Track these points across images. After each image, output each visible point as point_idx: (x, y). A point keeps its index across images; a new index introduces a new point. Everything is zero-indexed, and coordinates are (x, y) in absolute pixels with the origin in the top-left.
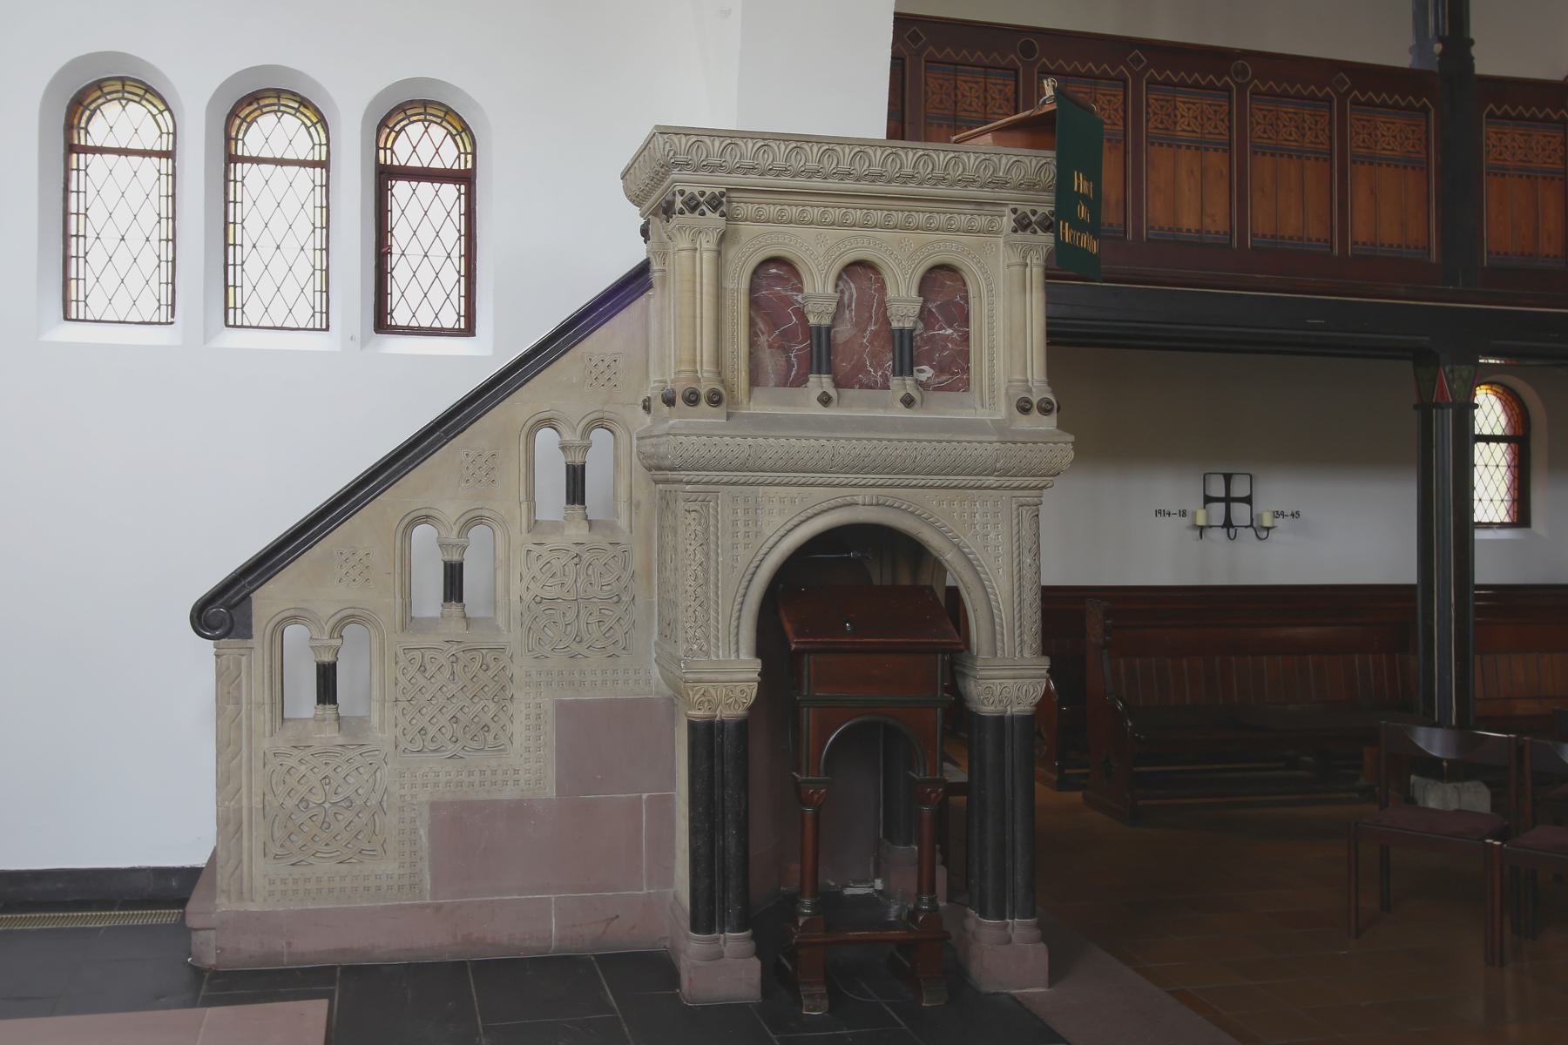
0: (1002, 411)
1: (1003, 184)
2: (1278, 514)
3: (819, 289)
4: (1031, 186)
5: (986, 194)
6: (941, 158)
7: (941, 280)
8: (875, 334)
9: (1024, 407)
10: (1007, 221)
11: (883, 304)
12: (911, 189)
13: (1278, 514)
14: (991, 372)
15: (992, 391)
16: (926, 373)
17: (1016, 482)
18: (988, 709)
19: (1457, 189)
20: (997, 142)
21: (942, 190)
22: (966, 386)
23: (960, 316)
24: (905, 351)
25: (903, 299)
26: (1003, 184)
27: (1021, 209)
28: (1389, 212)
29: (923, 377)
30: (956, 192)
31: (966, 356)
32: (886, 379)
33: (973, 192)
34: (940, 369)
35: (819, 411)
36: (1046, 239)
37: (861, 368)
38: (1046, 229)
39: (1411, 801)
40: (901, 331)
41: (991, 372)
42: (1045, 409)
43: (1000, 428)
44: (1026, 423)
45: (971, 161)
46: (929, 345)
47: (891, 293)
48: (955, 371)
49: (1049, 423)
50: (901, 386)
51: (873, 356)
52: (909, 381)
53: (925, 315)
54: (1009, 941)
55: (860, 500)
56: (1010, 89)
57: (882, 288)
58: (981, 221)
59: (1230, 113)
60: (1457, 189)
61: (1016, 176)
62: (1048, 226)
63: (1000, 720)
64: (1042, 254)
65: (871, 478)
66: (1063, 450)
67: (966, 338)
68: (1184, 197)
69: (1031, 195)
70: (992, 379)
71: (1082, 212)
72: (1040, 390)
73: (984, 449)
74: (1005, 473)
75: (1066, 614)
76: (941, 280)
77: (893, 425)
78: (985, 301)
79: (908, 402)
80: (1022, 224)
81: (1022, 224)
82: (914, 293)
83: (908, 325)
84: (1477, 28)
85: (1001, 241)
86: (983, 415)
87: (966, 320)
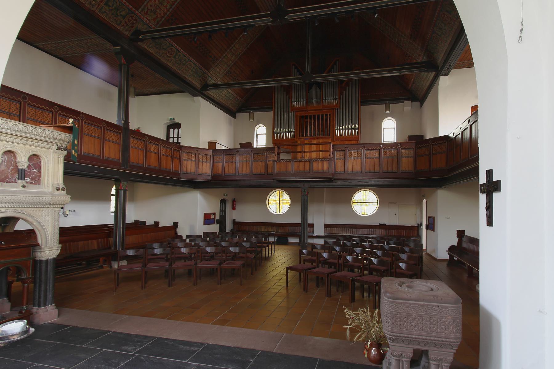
0: (50, 190)
1: (55, 139)
2: (70, 211)
3: (23, 160)
4: (62, 140)
5: (50, 140)
6: (39, 130)
7: (34, 159)
8: (13, 169)
9: (58, 189)
10: (55, 147)
11: (15, 162)
12: (29, 136)
13: (70, 211)
14: (48, 181)
15: (48, 185)
16: (28, 180)
17: (56, 206)
18: (44, 258)
19: (126, 149)
20: (54, 129)
21: (38, 137)
22: (39, 183)
23: (39, 167)
24: (22, 174)
25: (23, 162)
26: (55, 139)
27: (59, 145)
28: (112, 152)
29: (27, 181)
30: (42, 138)
31: (40, 177)
32: (16, 180)
33: (47, 139)
34: (32, 179)
35: (22, 189)
36: (65, 153)
37: (8, 177)
38: (65, 150)
39: (111, 267)
40: (22, 169)
41: (48, 181)
42: (63, 190)
43: (52, 194)
44: (58, 193)
45: (48, 132)
46: (31, 172)
47: (18, 159)
48: (37, 180)
49: (64, 193)
50: (21, 183)
51: (12, 175)
52: (24, 181)
53: (29, 167)
54: (47, 311)
55: (8, 211)
56: (18, 106)
57: (15, 158)
58: (48, 146)
59: (52, 117)
60: (126, 149)
61: (59, 137)
62: (65, 149)
63: (47, 261)
64: (64, 155)
65: (12, 205)
66: (68, 198)
67: (40, 172)
68: (91, 147)
69: (62, 142)
70: (48, 182)
71: (76, 148)
72: (62, 186)
73: (49, 199)
74: (52, 204)
75: (67, 234)
76: (34, 159)
77: (20, 192)
78: (47, 164)
79: (24, 187)
80: (59, 148)
81: (59, 148)
82: (26, 160)
83: (24, 168)
84: (130, 120)
85: (52, 151)
86: (45, 190)
87: (40, 168)
